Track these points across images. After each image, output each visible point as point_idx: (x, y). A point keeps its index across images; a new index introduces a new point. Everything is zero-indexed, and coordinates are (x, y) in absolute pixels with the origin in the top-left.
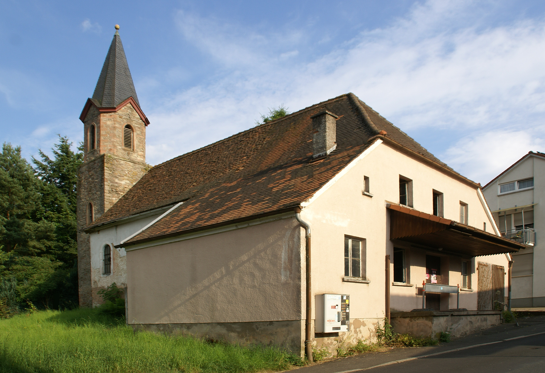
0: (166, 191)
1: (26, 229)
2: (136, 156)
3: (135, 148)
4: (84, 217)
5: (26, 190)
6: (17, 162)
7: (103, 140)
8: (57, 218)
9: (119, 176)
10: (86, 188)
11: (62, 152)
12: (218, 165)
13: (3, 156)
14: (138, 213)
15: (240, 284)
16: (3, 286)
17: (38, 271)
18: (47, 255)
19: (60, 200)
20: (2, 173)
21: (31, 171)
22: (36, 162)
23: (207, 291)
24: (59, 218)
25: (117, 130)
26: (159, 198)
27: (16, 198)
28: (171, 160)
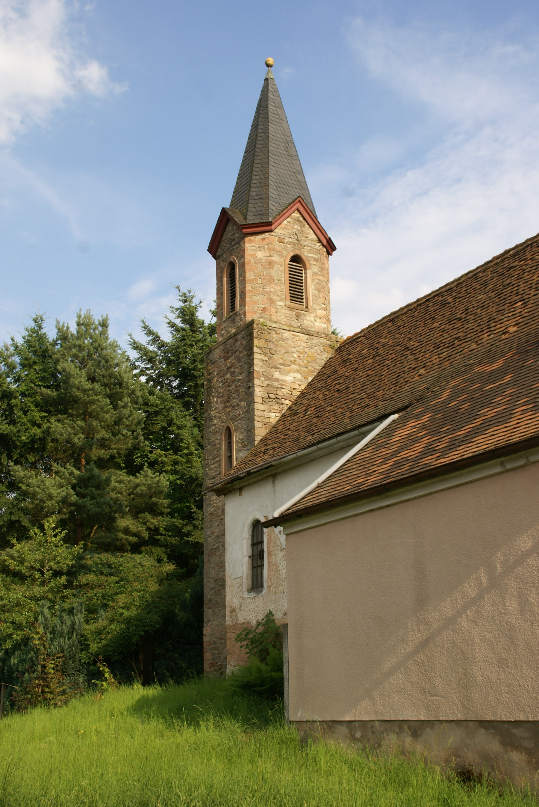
0: (368, 392)
1: (113, 490)
2: (312, 319)
3: (311, 303)
4: (217, 459)
5: (115, 408)
6: (102, 349)
7: (251, 291)
8: (171, 464)
9: (281, 364)
10: (221, 395)
11: (184, 321)
12: (467, 327)
13: (77, 338)
14: (314, 445)
15: (522, 613)
16: (58, 626)
17: (126, 586)
18: (150, 549)
19: (178, 423)
20: (73, 373)
21: (127, 367)
22: (136, 346)
23: (451, 632)
24: (175, 463)
25: (275, 269)
26: (354, 408)
27: (97, 424)
28: (376, 323)
